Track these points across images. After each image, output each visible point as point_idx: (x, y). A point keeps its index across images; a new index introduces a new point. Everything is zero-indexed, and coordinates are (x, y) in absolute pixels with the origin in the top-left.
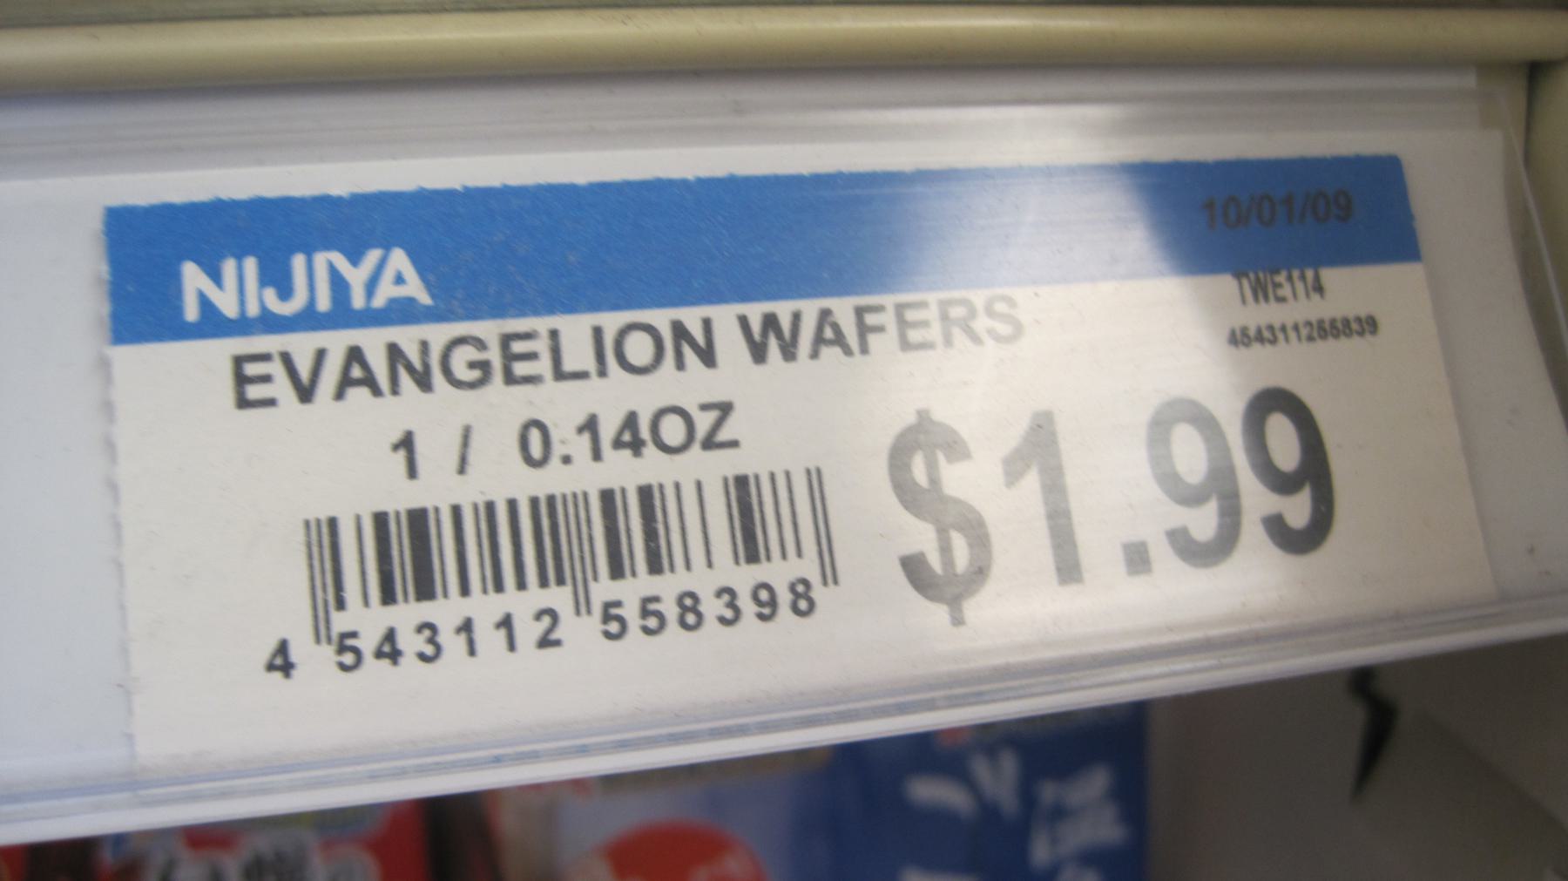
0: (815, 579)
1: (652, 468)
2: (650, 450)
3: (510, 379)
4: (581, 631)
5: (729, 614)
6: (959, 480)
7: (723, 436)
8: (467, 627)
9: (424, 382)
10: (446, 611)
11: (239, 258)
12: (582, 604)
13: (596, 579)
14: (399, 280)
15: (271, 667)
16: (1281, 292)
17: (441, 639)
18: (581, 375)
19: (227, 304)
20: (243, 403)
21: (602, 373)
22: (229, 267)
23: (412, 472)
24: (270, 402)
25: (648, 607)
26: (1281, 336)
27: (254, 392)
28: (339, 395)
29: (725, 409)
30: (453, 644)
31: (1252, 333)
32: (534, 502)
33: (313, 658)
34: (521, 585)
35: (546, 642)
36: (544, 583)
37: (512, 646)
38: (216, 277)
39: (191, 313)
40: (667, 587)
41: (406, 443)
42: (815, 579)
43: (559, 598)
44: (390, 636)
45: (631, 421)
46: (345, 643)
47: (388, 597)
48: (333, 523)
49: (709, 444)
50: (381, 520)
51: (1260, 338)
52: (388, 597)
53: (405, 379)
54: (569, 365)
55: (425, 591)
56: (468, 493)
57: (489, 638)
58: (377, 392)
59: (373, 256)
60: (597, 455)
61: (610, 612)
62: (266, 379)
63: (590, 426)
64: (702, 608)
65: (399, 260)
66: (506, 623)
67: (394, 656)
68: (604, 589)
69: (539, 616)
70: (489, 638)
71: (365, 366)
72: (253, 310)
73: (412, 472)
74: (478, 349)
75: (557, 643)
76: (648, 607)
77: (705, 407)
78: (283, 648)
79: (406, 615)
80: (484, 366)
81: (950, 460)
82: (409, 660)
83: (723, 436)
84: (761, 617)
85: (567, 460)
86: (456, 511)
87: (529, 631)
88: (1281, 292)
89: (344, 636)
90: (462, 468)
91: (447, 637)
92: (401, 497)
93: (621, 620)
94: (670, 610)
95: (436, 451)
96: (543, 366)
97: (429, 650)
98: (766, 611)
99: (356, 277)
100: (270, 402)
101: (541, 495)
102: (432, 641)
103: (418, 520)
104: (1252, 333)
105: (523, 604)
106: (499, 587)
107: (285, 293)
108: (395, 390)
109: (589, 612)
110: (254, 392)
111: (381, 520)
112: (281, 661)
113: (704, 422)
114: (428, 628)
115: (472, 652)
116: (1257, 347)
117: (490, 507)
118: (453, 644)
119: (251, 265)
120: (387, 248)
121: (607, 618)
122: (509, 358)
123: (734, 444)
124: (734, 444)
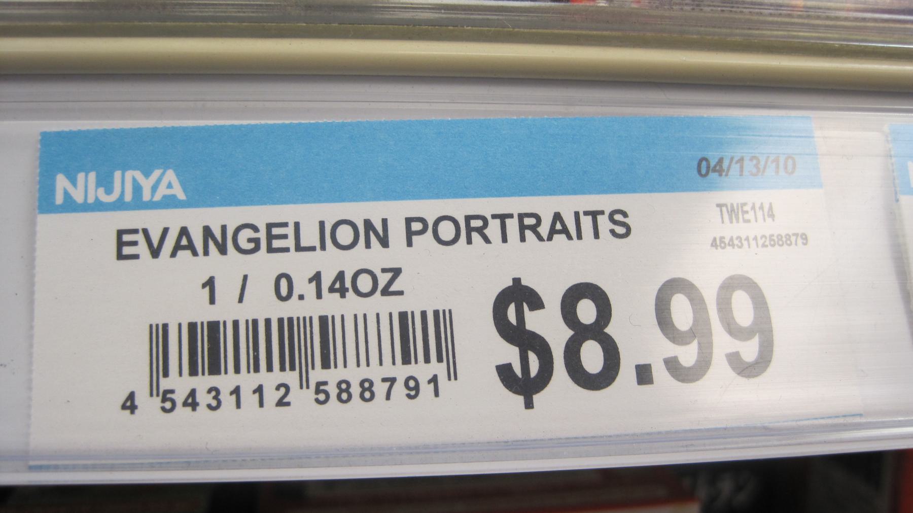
1: (351, 305)
2: (350, 294)
3: (270, 250)
4: (301, 398)
5: (214, 403)
6: (534, 321)
7: (394, 288)
8: (236, 391)
9: (223, 250)
10: (225, 382)
12: (304, 382)
13: (313, 368)
14: (170, 186)
15: (124, 407)
16: (746, 217)
18: (313, 249)
20: (120, 256)
21: (323, 247)
22: (81, 177)
23: (212, 301)
24: (136, 257)
26: (745, 243)
27: (127, 250)
28: (173, 255)
29: (397, 272)
30: (228, 401)
31: (727, 241)
32: (281, 321)
33: (148, 405)
34: (270, 368)
35: (281, 403)
36: (283, 369)
37: (261, 404)
40: (332, 376)
41: (210, 284)
43: (291, 378)
44: (193, 393)
45: (341, 276)
46: (167, 395)
47: (193, 372)
48: (165, 326)
49: (386, 292)
50: (192, 327)
51: (731, 244)
52: (193, 372)
54: (304, 243)
55: (215, 369)
56: (245, 313)
59: (157, 173)
60: (319, 296)
61: (320, 388)
62: (135, 243)
63: (317, 278)
65: (170, 175)
66: (259, 390)
68: (317, 374)
69: (278, 388)
73: (212, 301)
75: (288, 404)
77: (384, 270)
78: (131, 396)
79: (203, 382)
80: (257, 241)
81: (532, 309)
82: (202, 409)
83: (394, 288)
85: (301, 297)
86: (236, 324)
87: (271, 396)
88: (746, 217)
91: (225, 397)
92: (204, 314)
94: (333, 390)
95: (227, 290)
96: (290, 243)
98: (413, 393)
99: (146, 184)
100: (136, 257)
102: (216, 398)
103: (214, 327)
104: (727, 241)
105: (270, 380)
107: (109, 191)
108: (206, 253)
109: (308, 387)
110: (127, 250)
111: (192, 327)
112: (130, 404)
113: (383, 279)
114: (215, 391)
116: (729, 248)
117: (255, 322)
118: (228, 401)
119: (92, 176)
121: (318, 391)
122: (270, 237)
123: (401, 293)
124: (401, 293)
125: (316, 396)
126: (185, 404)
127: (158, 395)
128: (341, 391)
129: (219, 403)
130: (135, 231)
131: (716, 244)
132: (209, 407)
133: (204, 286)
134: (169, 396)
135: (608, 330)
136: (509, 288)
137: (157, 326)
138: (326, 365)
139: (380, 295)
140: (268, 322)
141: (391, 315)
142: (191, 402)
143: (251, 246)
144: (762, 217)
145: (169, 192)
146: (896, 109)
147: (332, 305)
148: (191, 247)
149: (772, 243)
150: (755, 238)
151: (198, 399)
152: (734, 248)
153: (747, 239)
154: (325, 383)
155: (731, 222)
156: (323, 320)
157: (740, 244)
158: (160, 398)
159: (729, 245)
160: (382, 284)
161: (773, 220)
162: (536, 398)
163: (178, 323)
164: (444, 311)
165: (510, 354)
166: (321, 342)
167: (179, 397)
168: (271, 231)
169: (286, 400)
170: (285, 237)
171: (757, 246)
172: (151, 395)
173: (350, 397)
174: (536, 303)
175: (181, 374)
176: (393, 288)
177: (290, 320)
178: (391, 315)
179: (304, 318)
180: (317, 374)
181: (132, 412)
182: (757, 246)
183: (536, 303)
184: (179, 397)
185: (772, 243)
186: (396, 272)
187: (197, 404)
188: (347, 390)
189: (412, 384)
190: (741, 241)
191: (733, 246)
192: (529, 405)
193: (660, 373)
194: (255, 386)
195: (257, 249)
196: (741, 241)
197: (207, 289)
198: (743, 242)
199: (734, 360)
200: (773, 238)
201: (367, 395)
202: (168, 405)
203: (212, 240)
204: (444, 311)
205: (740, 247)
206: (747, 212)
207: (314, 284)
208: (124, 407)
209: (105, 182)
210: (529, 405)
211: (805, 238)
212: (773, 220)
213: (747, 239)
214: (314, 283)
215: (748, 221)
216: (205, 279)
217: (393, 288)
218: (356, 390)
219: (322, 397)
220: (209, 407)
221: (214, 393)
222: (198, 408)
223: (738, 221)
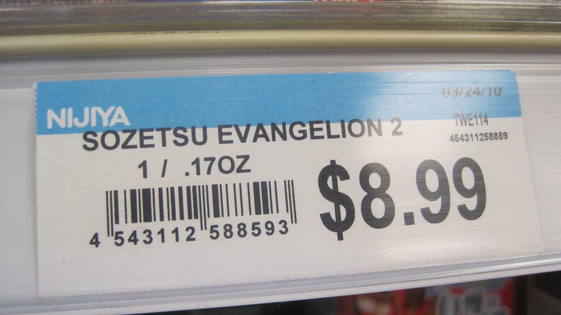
0: (288, 220)
3: (313, 137)
4: (202, 235)
5: (284, 230)
6: (344, 187)
7: (244, 168)
8: (162, 232)
9: (284, 137)
10: (155, 226)
11: (67, 108)
12: (203, 226)
13: (209, 217)
14: (120, 117)
15: (91, 243)
16: (471, 122)
17: (152, 236)
18: (338, 137)
19: (61, 123)
20: (221, 141)
21: (344, 136)
22: (63, 111)
23: (145, 176)
24: (231, 142)
25: (255, 226)
26: (470, 138)
27: (225, 138)
28: (255, 140)
29: (246, 158)
30: (157, 238)
31: (459, 137)
32: (188, 188)
33: (107, 241)
34: (182, 218)
35: (189, 239)
36: (190, 217)
37: (177, 240)
38: (59, 115)
39: (50, 125)
40: (221, 222)
41: (144, 165)
42: (288, 220)
43: (195, 223)
44: (134, 234)
46: (118, 235)
47: (134, 220)
48: (116, 192)
49: (239, 170)
50: (133, 192)
52: (134, 220)
53: (277, 135)
54: (333, 133)
55: (148, 218)
56: (166, 183)
57: (170, 236)
58: (268, 140)
59: (111, 109)
62: (230, 134)
64: (232, 230)
66: (176, 231)
67: (135, 241)
68: (211, 221)
69: (187, 229)
70: (170, 236)
71: (264, 131)
72: (70, 125)
73: (145, 176)
74: (303, 127)
75: (194, 239)
76: (255, 226)
77: (238, 157)
78: (96, 236)
79: (140, 227)
80: (304, 132)
81: (342, 179)
82: (140, 243)
83: (244, 168)
84: (268, 233)
86: (160, 190)
87: (183, 235)
88: (471, 122)
89: (118, 233)
90: (163, 175)
92: (140, 184)
93: (259, 229)
94: (221, 230)
95: (154, 169)
96: (324, 133)
97: (148, 240)
98: (270, 231)
99: (105, 116)
100: (231, 142)
101: (260, 181)
102: (149, 236)
103: (146, 192)
104: (459, 137)
105: (182, 225)
106: (174, 219)
107: (81, 120)
108: (274, 139)
109: (206, 228)
110: (225, 138)
111: (133, 192)
113: (238, 162)
115: (163, 241)
116: (460, 142)
117: (172, 189)
118: (157, 238)
119: (70, 110)
120: (117, 106)
121: (212, 231)
122: (312, 130)
123: (249, 171)
124: (249, 171)
125: (253, 231)
126: (130, 240)
127: (112, 235)
128: (226, 231)
129: (151, 240)
130: (230, 126)
131: (453, 139)
132: (145, 242)
133: (193, 164)
134: (119, 235)
135: (387, 192)
136: (328, 166)
137: (111, 192)
138: (217, 215)
139: (236, 173)
140: (180, 189)
141: (248, 184)
142: (134, 239)
143: (301, 135)
144: (480, 123)
145: (120, 121)
146: (486, 62)
147: (217, 178)
148: (265, 135)
149: (486, 138)
150: (476, 135)
151: (138, 238)
152: (463, 141)
153: (471, 135)
154: (217, 226)
155: (462, 125)
156: (215, 187)
157: (467, 139)
158: (114, 237)
159: (461, 139)
160: (237, 165)
161: (487, 124)
162: (345, 233)
163: (106, 191)
164: (199, 186)
165: (329, 207)
166: (213, 199)
167: (126, 236)
168: (143, 134)
169: (193, 237)
170: (321, 129)
171: (478, 140)
172: (109, 235)
173: (232, 234)
174: (345, 176)
175: (237, 215)
176: (243, 168)
177: (194, 187)
178: (248, 184)
179: (203, 186)
180: (211, 221)
181: (97, 246)
182: (478, 140)
183: (345, 176)
184: (126, 236)
185: (457, 139)
186: (246, 158)
187: (138, 240)
188: (230, 230)
189: (269, 226)
190: (467, 137)
191: (463, 140)
192: (340, 238)
193: (418, 217)
194: (174, 229)
195: (305, 137)
196: (467, 137)
197: (142, 168)
198: (469, 137)
199: (463, 210)
200: (501, 134)
201: (242, 233)
202: (119, 241)
203: (277, 131)
204: (199, 186)
205: (467, 141)
206: (471, 119)
207: (142, 168)
208: (91, 243)
209: (79, 115)
210: (340, 238)
211: (506, 134)
212: (487, 124)
213: (471, 135)
214: (142, 168)
215: (472, 125)
216: (140, 162)
217: (243, 168)
218: (235, 230)
219: (214, 235)
220: (281, 232)
221: (147, 233)
222: (138, 243)
223: (466, 125)
